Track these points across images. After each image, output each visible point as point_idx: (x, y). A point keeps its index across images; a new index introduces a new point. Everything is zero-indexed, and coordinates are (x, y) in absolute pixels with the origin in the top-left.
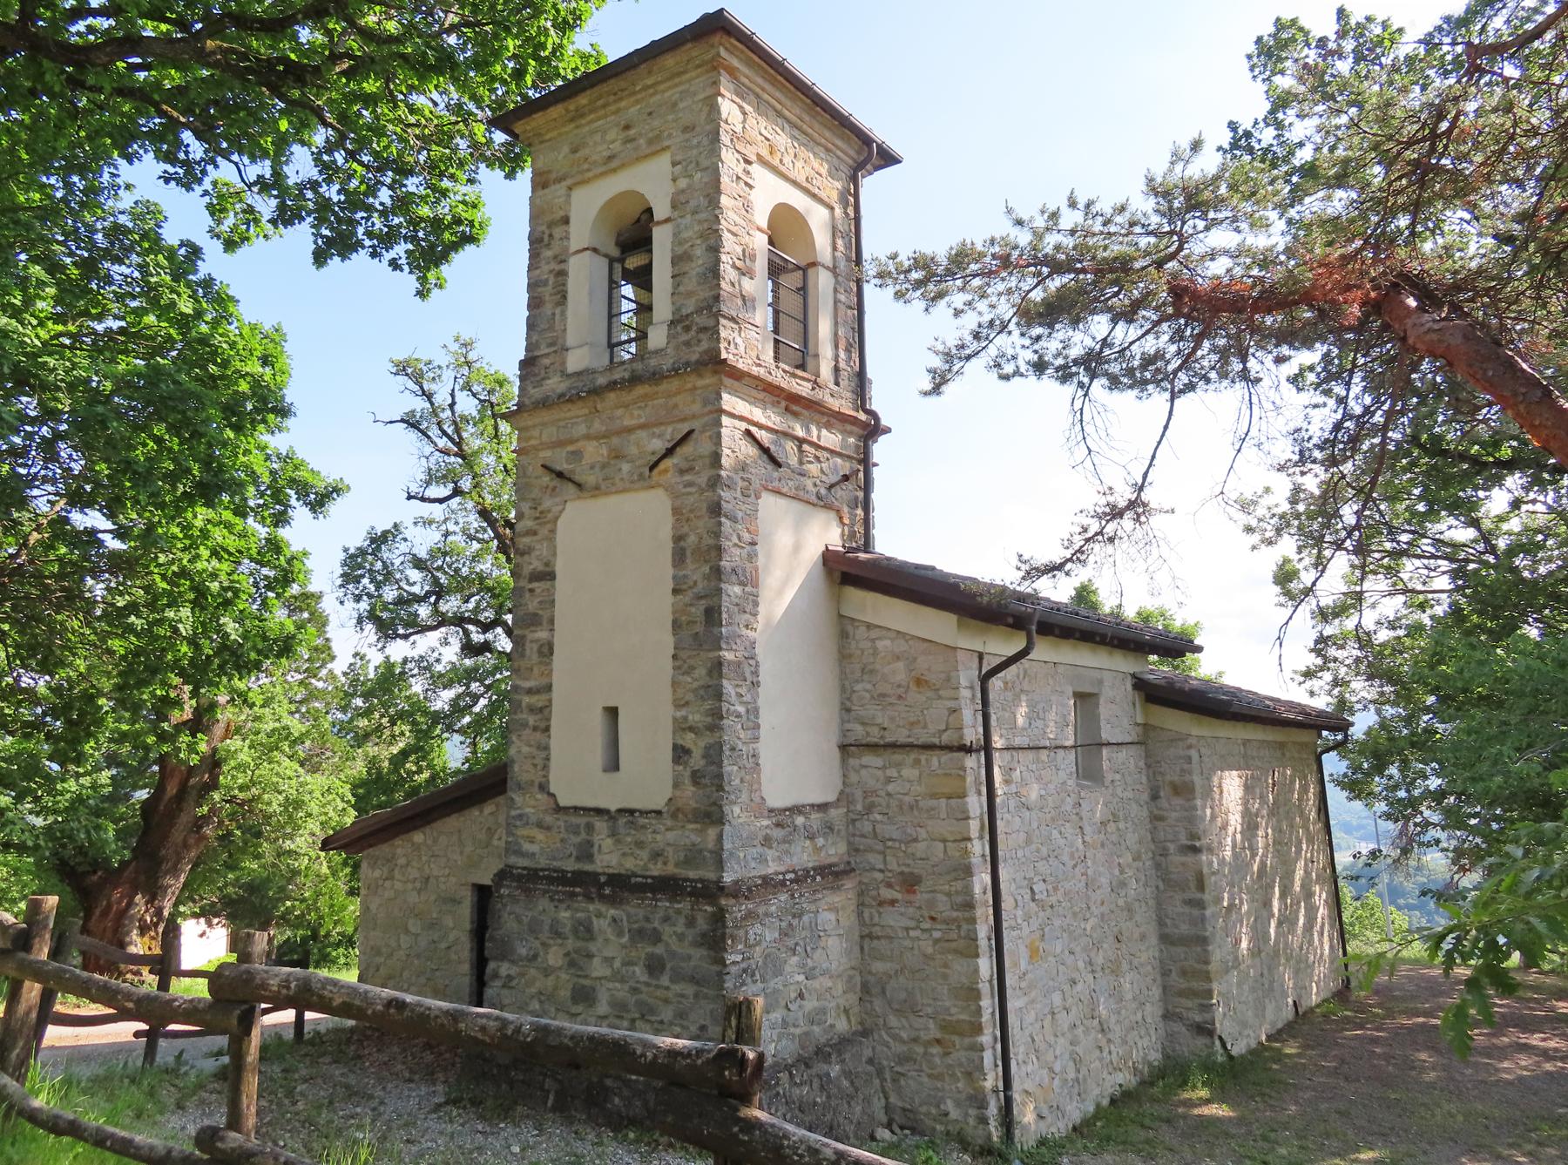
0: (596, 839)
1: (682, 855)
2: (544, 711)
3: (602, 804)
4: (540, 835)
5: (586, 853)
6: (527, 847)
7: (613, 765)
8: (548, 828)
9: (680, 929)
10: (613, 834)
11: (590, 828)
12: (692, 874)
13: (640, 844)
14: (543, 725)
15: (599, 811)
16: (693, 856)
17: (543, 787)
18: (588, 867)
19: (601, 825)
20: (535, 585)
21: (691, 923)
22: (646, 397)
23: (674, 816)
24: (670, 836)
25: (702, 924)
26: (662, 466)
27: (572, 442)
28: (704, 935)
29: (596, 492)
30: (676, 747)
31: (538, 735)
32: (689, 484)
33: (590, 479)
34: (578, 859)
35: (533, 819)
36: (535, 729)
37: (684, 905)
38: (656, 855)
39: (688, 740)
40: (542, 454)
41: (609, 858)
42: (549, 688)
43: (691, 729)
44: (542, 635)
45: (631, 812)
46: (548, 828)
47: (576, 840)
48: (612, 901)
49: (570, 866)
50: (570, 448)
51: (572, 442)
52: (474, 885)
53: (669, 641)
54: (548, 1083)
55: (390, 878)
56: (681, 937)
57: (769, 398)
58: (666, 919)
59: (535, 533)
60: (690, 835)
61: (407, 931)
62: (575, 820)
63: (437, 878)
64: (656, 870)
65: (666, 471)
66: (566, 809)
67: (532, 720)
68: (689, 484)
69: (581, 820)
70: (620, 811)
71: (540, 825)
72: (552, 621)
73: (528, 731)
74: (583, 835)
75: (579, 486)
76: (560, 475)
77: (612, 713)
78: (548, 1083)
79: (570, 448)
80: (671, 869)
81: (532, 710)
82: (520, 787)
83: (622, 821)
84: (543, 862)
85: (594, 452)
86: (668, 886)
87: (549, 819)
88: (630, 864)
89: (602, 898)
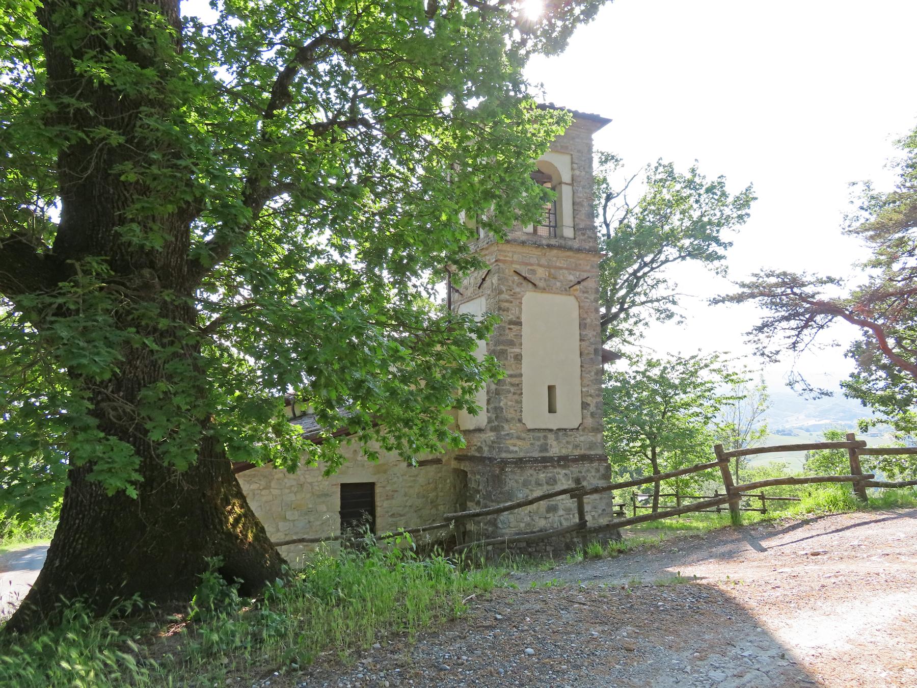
0: (549, 442)
1: (588, 446)
2: (518, 385)
3: (550, 427)
4: (519, 443)
5: (544, 448)
6: (512, 448)
7: (552, 410)
8: (524, 439)
9: (593, 474)
10: (557, 439)
11: (545, 437)
12: (592, 453)
13: (568, 442)
14: (519, 392)
15: (551, 430)
16: (592, 446)
17: (520, 421)
18: (548, 455)
19: (551, 436)
20: (512, 326)
21: (598, 470)
22: (569, 257)
23: (583, 430)
24: (582, 439)
25: (602, 470)
26: (575, 288)
27: (531, 265)
28: (603, 475)
29: (544, 290)
30: (583, 403)
31: (516, 397)
32: (587, 298)
33: (541, 284)
34: (541, 451)
35: (515, 435)
36: (514, 394)
37: (595, 464)
38: (576, 447)
39: (589, 400)
40: (514, 266)
41: (555, 450)
42: (521, 375)
43: (591, 396)
44: (517, 350)
45: (565, 430)
46: (524, 439)
47: (539, 443)
48: (564, 467)
49: (536, 454)
50: (530, 267)
51: (531, 265)
52: (342, 485)
53: (578, 360)
54: (548, 548)
55: (268, 487)
56: (594, 477)
57: (835, 306)
58: (588, 471)
59: (511, 302)
60: (591, 437)
61: (285, 519)
62: (537, 434)
63: (311, 484)
64: (577, 452)
65: (576, 290)
66: (529, 430)
67: (512, 389)
68: (587, 298)
69: (541, 435)
70: (559, 430)
71: (519, 438)
72: (521, 344)
73: (510, 395)
74: (542, 441)
75: (535, 285)
76: (525, 278)
77: (551, 389)
78: (548, 548)
79: (530, 267)
80: (583, 452)
81: (512, 385)
82: (507, 421)
83: (561, 434)
84: (522, 455)
85: (541, 272)
86: (584, 458)
87: (523, 435)
88: (564, 452)
89: (560, 466)
